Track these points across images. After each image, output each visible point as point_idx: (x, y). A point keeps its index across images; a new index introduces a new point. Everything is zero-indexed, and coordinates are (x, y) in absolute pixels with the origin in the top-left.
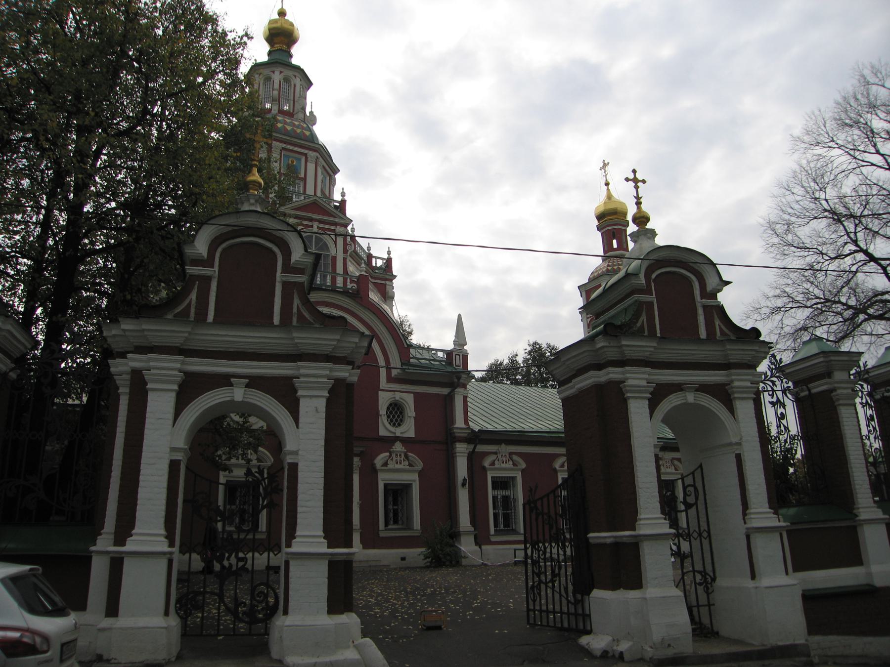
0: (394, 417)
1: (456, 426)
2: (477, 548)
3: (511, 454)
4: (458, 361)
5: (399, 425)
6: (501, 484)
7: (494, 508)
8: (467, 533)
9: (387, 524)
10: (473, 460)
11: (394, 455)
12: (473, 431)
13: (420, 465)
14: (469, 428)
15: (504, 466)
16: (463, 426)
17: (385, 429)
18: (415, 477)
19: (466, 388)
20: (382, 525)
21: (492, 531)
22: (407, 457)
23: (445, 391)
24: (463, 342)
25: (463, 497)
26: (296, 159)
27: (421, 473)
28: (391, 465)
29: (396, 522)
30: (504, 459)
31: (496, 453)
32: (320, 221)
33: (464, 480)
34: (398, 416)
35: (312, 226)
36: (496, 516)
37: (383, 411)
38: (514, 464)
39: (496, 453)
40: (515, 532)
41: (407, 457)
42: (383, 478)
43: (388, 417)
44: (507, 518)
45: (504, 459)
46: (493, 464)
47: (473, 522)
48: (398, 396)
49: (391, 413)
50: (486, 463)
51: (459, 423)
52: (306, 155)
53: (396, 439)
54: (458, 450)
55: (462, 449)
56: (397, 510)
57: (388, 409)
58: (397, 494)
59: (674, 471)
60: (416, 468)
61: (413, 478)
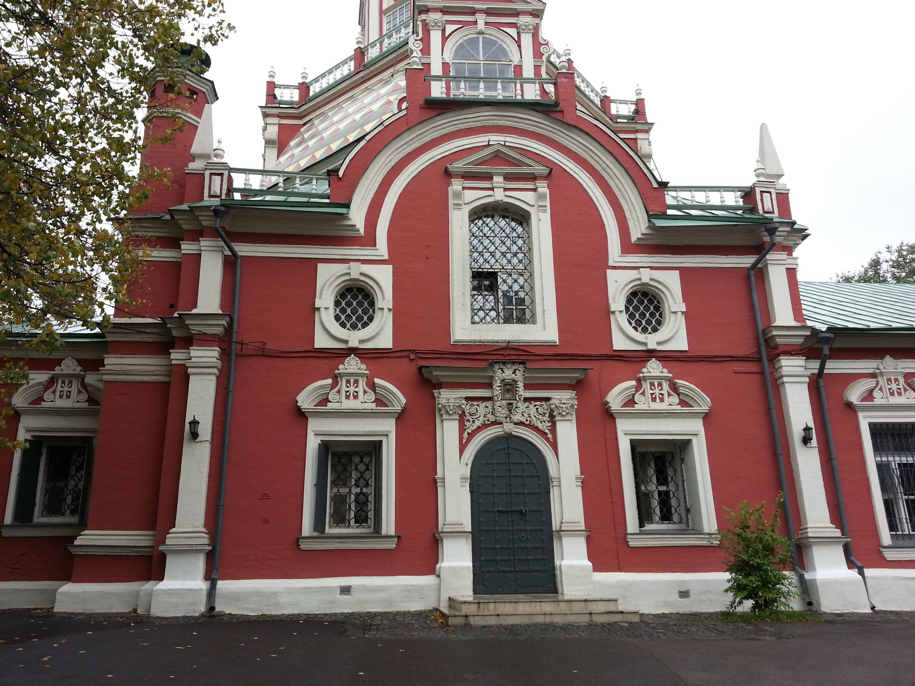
0: (643, 315)
1: (779, 322)
2: (854, 574)
5: (655, 330)
7: (884, 488)
9: (644, 516)
11: (646, 386)
12: (814, 331)
13: (704, 404)
17: (623, 336)
18: (388, 426)
20: (307, 528)
22: (674, 388)
23: (747, 261)
27: (400, 418)
28: (643, 403)
29: (666, 517)
30: (894, 387)
31: (873, 376)
32: (489, 12)
33: (807, 429)
35: (476, 23)
37: (617, 302)
39: (873, 376)
41: (674, 388)
42: (627, 431)
43: (632, 316)
45: (894, 387)
46: (869, 396)
47: (837, 516)
48: (646, 276)
49: (637, 309)
51: (783, 315)
53: (651, 354)
54: (785, 371)
55: (795, 372)
56: (667, 493)
57: (629, 301)
58: (661, 461)
60: (697, 409)
61: (692, 428)
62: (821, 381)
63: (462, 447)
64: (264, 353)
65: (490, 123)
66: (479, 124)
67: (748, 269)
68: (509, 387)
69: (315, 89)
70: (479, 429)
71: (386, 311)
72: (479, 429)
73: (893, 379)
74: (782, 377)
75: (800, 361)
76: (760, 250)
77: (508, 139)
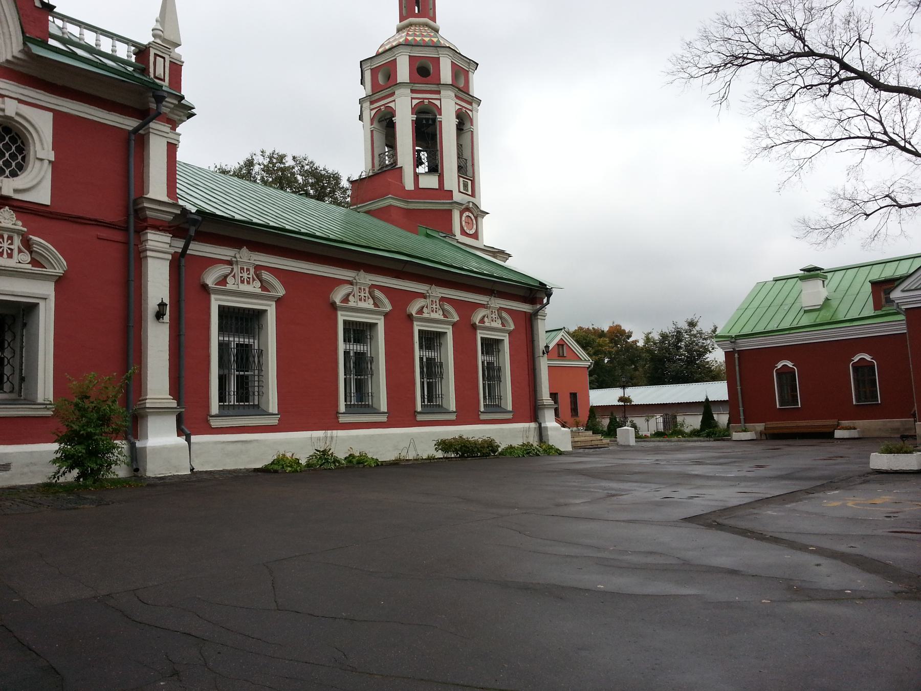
1: (151, 195)
2: (182, 441)
3: (258, 268)
4: (159, 69)
6: (241, 321)
8: (162, 411)
10: (180, 266)
12: (184, 210)
13: (59, 266)
14: (176, 205)
15: (362, 305)
16: (165, 199)
18: (47, 289)
19: (174, 128)
21: (215, 408)
23: (129, 123)
24: (172, 38)
25: (157, 340)
27: (59, 282)
30: (245, 275)
31: (230, 263)
33: (162, 305)
34: (13, 157)
36: (223, 380)
38: (263, 288)
39: (230, 263)
40: (259, 410)
41: (27, 244)
44: (244, 386)
45: (245, 275)
46: (223, 281)
47: (176, 388)
50: (211, 278)
51: (157, 190)
55: (159, 247)
59: (372, 307)
60: (50, 271)
62: (183, 261)
67: (129, 132)
71: (46, 162)
74: (146, 250)
75: (166, 238)
76: (145, 115)
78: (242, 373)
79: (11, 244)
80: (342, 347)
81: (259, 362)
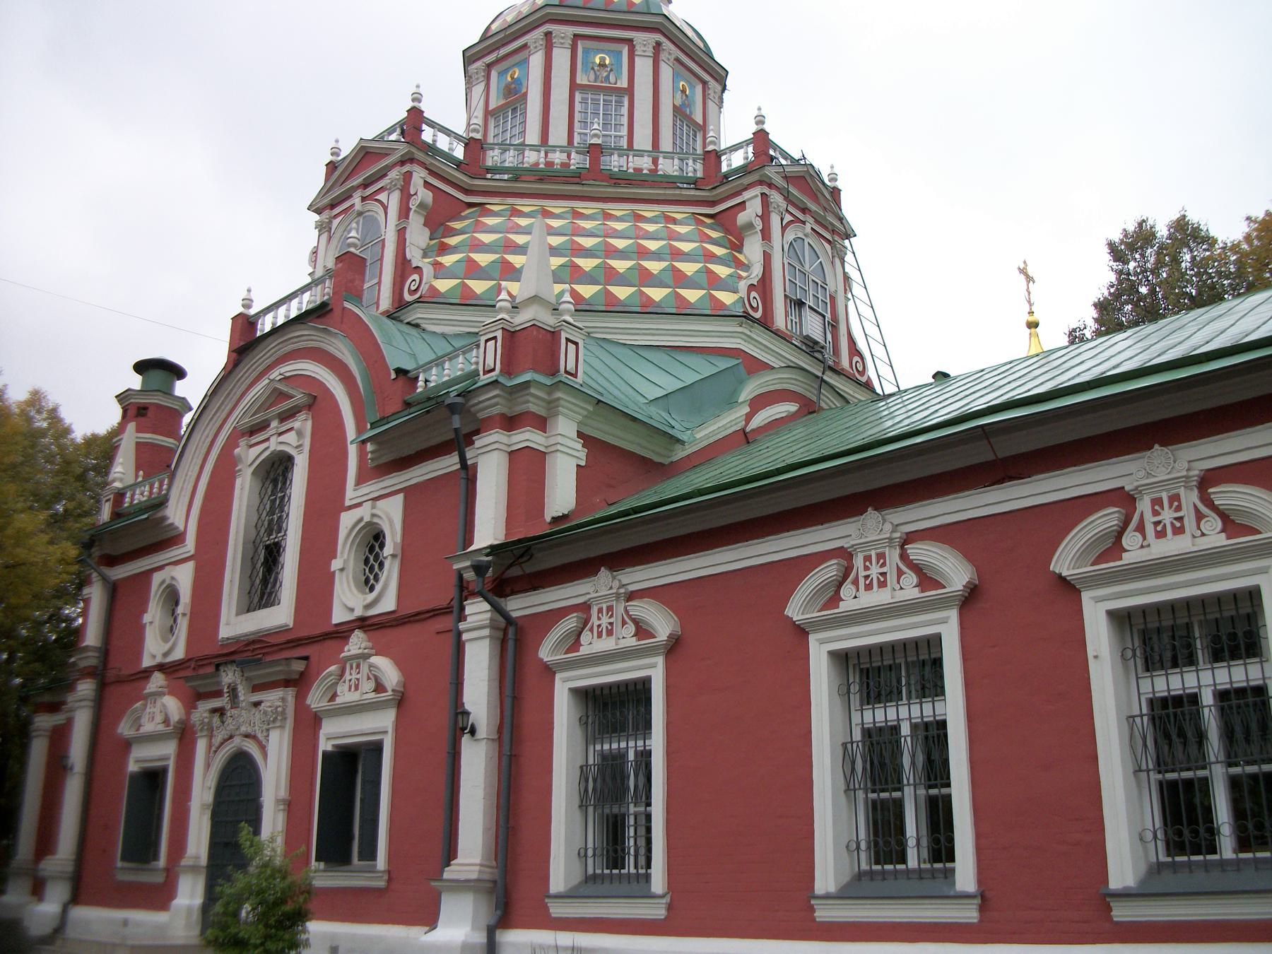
23: (449, 463)
26: (608, 52)
27: (401, 701)
52: (629, 42)
63: (208, 766)
64: (120, 681)
65: (280, 353)
66: (273, 359)
68: (233, 691)
69: (266, 325)
70: (222, 744)
72: (222, 744)
73: (1165, 496)
76: (460, 442)
77: (282, 370)
78: (884, 795)
79: (884, 565)
80: (657, 742)
81: (587, 781)
